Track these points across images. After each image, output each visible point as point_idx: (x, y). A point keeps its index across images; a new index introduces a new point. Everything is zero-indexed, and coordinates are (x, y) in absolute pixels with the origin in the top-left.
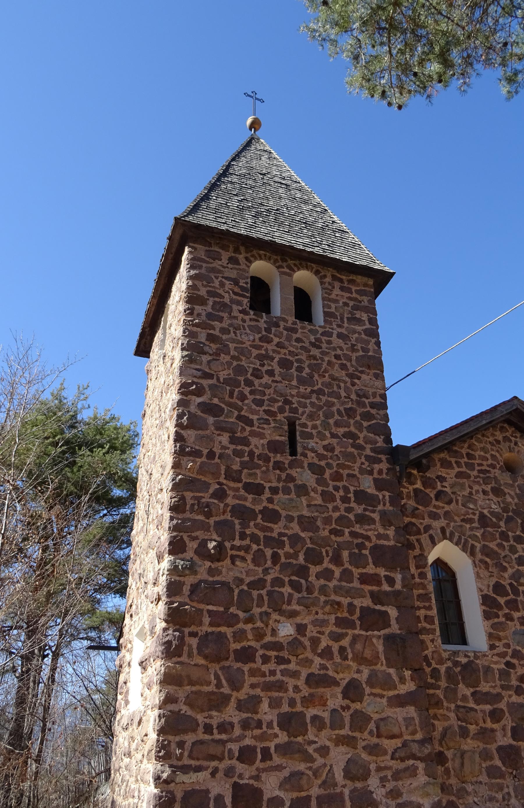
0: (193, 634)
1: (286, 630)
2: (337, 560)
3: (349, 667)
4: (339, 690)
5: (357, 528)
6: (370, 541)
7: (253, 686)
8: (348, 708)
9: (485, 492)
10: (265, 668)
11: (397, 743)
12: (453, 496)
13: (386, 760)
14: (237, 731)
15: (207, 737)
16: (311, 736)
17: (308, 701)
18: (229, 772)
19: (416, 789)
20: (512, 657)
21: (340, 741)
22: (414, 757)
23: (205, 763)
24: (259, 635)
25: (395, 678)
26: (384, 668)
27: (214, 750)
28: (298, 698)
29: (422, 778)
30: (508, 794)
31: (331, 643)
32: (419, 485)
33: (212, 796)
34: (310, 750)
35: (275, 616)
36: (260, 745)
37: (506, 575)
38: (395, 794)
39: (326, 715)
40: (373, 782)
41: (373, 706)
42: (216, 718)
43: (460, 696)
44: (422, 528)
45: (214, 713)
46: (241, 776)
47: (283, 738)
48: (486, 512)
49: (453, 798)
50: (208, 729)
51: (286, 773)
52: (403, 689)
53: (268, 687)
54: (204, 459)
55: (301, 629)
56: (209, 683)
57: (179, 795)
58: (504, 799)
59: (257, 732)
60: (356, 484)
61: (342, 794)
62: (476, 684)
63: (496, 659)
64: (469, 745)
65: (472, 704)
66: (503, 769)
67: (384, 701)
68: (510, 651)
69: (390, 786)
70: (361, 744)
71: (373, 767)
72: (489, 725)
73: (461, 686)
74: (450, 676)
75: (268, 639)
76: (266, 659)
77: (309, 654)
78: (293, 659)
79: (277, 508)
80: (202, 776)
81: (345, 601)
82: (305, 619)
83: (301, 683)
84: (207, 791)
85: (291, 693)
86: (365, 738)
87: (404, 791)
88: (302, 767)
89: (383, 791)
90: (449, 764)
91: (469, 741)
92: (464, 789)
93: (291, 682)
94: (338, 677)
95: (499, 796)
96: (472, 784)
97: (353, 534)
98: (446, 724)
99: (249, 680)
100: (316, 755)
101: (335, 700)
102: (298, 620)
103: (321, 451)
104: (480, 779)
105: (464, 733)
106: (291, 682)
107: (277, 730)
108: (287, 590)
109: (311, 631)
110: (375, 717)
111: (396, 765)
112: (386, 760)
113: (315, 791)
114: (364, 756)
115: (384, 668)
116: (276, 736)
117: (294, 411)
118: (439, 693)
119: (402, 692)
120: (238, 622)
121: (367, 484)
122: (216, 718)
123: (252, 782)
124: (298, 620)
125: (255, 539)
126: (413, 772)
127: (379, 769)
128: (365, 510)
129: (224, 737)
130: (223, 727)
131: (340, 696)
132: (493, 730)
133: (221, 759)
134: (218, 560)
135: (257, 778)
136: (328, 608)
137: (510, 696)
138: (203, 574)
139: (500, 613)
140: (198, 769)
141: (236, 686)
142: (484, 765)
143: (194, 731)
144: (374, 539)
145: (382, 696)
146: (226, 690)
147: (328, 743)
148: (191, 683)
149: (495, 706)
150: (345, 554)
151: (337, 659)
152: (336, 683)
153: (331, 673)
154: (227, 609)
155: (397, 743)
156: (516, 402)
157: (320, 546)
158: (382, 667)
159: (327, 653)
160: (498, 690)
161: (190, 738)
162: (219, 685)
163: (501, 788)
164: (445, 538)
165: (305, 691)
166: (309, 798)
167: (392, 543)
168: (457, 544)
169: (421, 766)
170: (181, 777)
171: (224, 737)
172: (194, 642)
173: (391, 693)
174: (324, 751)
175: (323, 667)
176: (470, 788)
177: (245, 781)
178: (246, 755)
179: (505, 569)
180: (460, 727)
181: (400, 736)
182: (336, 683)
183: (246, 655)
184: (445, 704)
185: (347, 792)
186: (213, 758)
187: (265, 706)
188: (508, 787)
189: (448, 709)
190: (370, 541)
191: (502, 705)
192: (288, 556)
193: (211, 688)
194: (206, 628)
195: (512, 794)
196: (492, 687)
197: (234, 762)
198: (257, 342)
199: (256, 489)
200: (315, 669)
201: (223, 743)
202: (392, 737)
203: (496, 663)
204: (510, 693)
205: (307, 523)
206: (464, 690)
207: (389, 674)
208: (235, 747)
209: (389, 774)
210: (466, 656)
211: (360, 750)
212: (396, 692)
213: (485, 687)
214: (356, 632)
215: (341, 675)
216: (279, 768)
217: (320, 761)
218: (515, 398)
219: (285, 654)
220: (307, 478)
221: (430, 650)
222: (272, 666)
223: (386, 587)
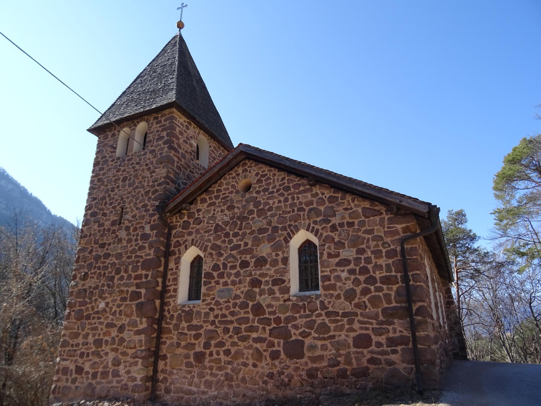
0: (73, 311)
1: (102, 305)
2: (126, 271)
3: (122, 319)
4: (116, 329)
5: (138, 253)
6: (143, 258)
7: (88, 329)
8: (118, 336)
9: (222, 211)
10: (93, 322)
11: (134, 351)
12: (202, 219)
13: (128, 359)
14: (81, 346)
15: (72, 349)
16: (103, 348)
17: (104, 334)
18: (76, 361)
19: (135, 371)
20: (214, 305)
21: (113, 350)
22: (137, 357)
23: (69, 358)
24: (93, 308)
25: (139, 322)
26: (135, 318)
27: (72, 353)
28: (102, 333)
29: (140, 366)
30: (194, 375)
31: (117, 309)
32: (186, 218)
33: (70, 369)
34: (102, 353)
35: (99, 300)
36: (87, 352)
37: (222, 259)
38: (128, 372)
39: (109, 339)
40: (121, 367)
41: (125, 335)
42: (76, 341)
43: (181, 327)
44: (182, 242)
45: (75, 340)
46: (79, 363)
47: (94, 349)
48: (220, 223)
49: (166, 376)
50: (72, 346)
51: (92, 362)
52: (141, 327)
53: (92, 329)
54: (88, 238)
55: (107, 304)
56: (75, 329)
57: (61, 368)
58: (191, 378)
59: (86, 347)
60: (142, 230)
61: (109, 371)
62: (191, 320)
63: (204, 307)
64: (179, 351)
65: (186, 331)
66: (194, 363)
67: (132, 333)
68: (213, 302)
69: (126, 369)
70: (120, 351)
71: (122, 361)
72: (193, 341)
73: (183, 322)
74: (179, 318)
75: (96, 310)
76: (94, 318)
77: (108, 315)
78: (102, 317)
79: (110, 252)
80: (68, 362)
81: (125, 289)
82: (109, 300)
83: (103, 327)
84: (69, 368)
85: (99, 331)
86: (121, 349)
87: (132, 371)
88: (97, 360)
89: (124, 371)
90: (168, 361)
91: (180, 349)
92: (172, 372)
93: (100, 327)
94: (117, 323)
95: (189, 376)
96: (176, 370)
97: (136, 257)
98: (172, 341)
99: (88, 327)
100: (103, 356)
101: (114, 332)
102: (107, 300)
103: (131, 219)
104: (182, 368)
105: (178, 345)
106: (100, 327)
107: (92, 346)
108: (106, 288)
109: (110, 305)
110: (128, 340)
111: (132, 360)
112: (128, 359)
113: (100, 370)
114: (120, 356)
115: (135, 318)
116: (92, 348)
117: (124, 202)
118: (171, 327)
119: (141, 328)
120: (87, 304)
121: (147, 230)
122: (76, 341)
123: (81, 365)
124: (107, 300)
125: (99, 268)
126: (136, 364)
127: (125, 362)
128: (143, 243)
129: (77, 348)
130: (77, 345)
131: (116, 331)
132: (195, 344)
133: (74, 356)
134: (85, 280)
135: (83, 364)
136: (118, 294)
137: (207, 326)
138: (80, 287)
139: (213, 281)
140: (67, 360)
141: (83, 330)
142: (185, 361)
143: (68, 346)
144: (144, 257)
145: (132, 331)
146: (80, 331)
147: (109, 351)
148: (70, 329)
149: (198, 332)
150: (130, 267)
151: (118, 315)
152: (116, 326)
153: (114, 322)
154: (84, 299)
155: (134, 351)
156: (241, 146)
157: (121, 266)
158: (134, 317)
159: (114, 314)
160: (202, 323)
161: (67, 349)
162: (78, 329)
163: (190, 372)
164: (192, 244)
165: (105, 330)
166: (98, 372)
167: (152, 257)
168: (197, 247)
169: (140, 361)
170: (62, 362)
171: (77, 348)
172: (73, 313)
173: (135, 329)
174: (107, 354)
175: (112, 320)
176: (175, 371)
177: (79, 365)
178: (82, 355)
179: (222, 255)
180: (177, 343)
181: (135, 347)
182: (116, 326)
183: (88, 317)
184: (173, 332)
185: (111, 370)
186: (71, 356)
187: (90, 336)
188: (195, 372)
189: (174, 334)
190: (143, 258)
191: (202, 331)
192: (109, 273)
193: (76, 331)
194: (78, 308)
195: (196, 376)
196: (198, 322)
197: (78, 358)
198: (115, 173)
199: (102, 246)
200: (109, 321)
201: (76, 351)
202: (131, 348)
203: (203, 309)
204: (207, 324)
205: (119, 256)
206: (184, 324)
207: (137, 321)
208: (79, 352)
209: (128, 364)
210: (189, 307)
211: (119, 354)
212: (137, 329)
213: (195, 322)
214: (127, 303)
215: (119, 322)
216: (91, 360)
217: (105, 358)
218: (241, 144)
219: (100, 315)
220: (123, 234)
221: (172, 305)
222: (95, 320)
223: (144, 280)
